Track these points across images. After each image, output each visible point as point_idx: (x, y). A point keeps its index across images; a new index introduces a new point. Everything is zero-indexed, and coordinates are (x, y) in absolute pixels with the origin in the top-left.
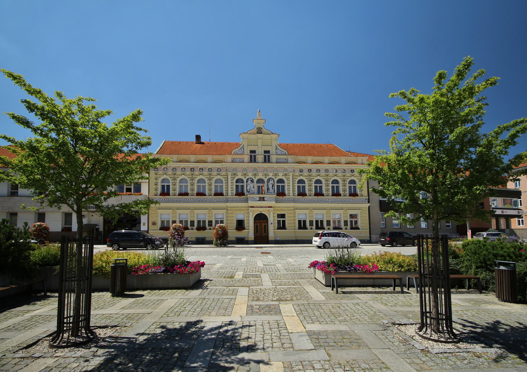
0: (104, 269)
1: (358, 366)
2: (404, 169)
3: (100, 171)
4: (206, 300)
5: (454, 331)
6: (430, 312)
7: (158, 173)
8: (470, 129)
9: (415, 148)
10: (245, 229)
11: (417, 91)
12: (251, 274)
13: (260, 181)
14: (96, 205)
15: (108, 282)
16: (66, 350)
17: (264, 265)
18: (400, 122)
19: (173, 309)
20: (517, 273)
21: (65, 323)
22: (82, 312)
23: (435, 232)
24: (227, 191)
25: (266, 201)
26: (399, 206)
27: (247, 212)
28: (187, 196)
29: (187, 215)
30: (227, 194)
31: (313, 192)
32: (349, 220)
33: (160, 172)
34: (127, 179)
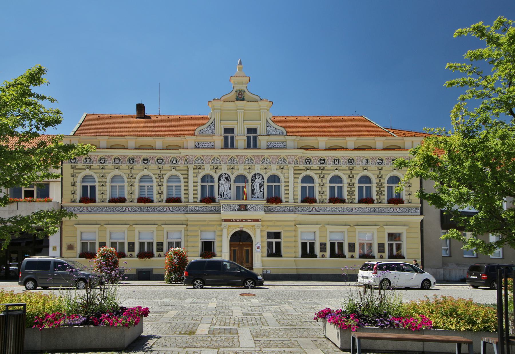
7: (77, 167)
9: (498, 123)
10: (215, 257)
12: (222, 329)
13: (241, 178)
24: (188, 194)
25: (250, 210)
26: (467, 221)
28: (123, 204)
30: (186, 200)
32: (386, 242)
33: (80, 165)
34: (24, 179)
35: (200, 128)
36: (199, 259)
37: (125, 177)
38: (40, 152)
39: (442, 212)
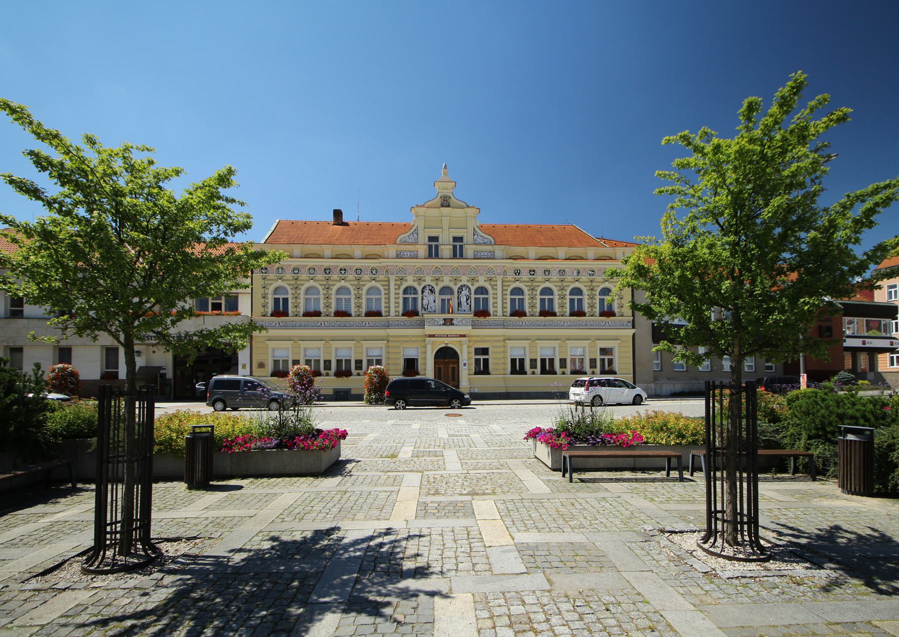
0: (174, 443)
1: (597, 599)
2: (684, 269)
3: (163, 273)
4: (348, 495)
5: (762, 542)
6: (723, 512)
7: (268, 278)
8: (800, 200)
11: (713, 132)
13: (446, 290)
14: (158, 333)
15: (181, 466)
16: (111, 577)
17: (449, 436)
18: (681, 188)
19: (291, 509)
20: (876, 446)
21: (108, 533)
22: (137, 514)
23: (735, 377)
24: (389, 307)
26: (677, 332)
27: (423, 344)
29: (318, 351)
30: (387, 314)
31: (538, 309)
32: (598, 357)
33: (272, 276)
34: (211, 289)
35: (402, 236)
36: (402, 377)
37: (320, 288)
38: (228, 260)
39: (653, 324)
